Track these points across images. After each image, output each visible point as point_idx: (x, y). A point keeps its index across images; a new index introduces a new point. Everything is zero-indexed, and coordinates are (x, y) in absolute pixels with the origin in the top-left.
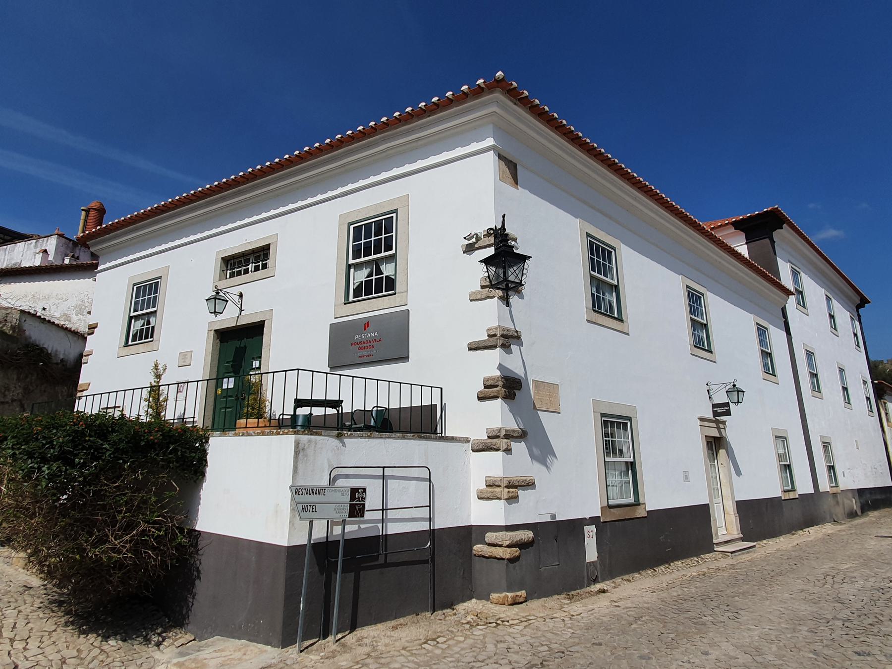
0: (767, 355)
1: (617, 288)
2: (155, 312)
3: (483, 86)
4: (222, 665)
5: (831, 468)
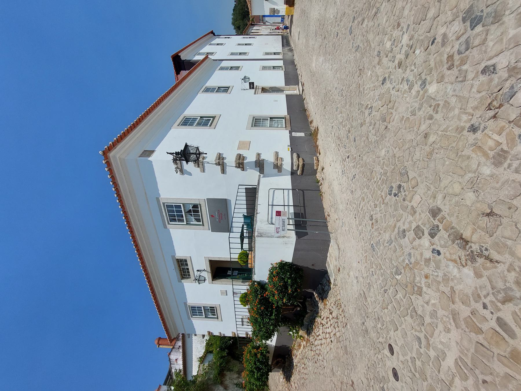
0: (232, 68)
1: (201, 117)
2: (204, 307)
3: (106, 161)
5: (275, 54)
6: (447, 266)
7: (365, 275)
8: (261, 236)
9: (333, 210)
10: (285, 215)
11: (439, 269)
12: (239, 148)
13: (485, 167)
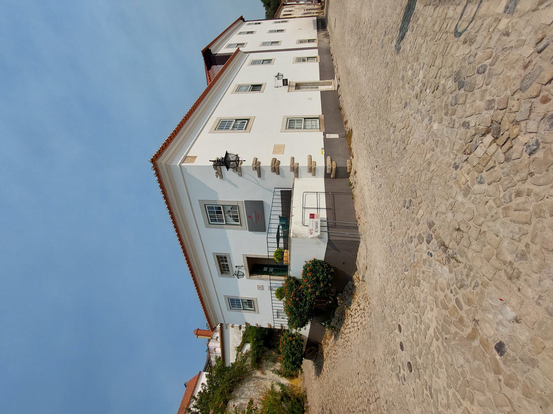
0: (264, 62)
1: (236, 120)
4: (339, 79)
5: (309, 41)
6: (435, 265)
7: (385, 272)
8: (296, 237)
9: (363, 213)
10: (317, 217)
11: (431, 266)
12: (274, 152)
13: (459, 196)
